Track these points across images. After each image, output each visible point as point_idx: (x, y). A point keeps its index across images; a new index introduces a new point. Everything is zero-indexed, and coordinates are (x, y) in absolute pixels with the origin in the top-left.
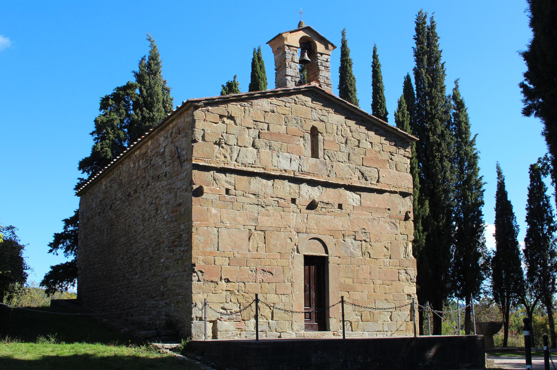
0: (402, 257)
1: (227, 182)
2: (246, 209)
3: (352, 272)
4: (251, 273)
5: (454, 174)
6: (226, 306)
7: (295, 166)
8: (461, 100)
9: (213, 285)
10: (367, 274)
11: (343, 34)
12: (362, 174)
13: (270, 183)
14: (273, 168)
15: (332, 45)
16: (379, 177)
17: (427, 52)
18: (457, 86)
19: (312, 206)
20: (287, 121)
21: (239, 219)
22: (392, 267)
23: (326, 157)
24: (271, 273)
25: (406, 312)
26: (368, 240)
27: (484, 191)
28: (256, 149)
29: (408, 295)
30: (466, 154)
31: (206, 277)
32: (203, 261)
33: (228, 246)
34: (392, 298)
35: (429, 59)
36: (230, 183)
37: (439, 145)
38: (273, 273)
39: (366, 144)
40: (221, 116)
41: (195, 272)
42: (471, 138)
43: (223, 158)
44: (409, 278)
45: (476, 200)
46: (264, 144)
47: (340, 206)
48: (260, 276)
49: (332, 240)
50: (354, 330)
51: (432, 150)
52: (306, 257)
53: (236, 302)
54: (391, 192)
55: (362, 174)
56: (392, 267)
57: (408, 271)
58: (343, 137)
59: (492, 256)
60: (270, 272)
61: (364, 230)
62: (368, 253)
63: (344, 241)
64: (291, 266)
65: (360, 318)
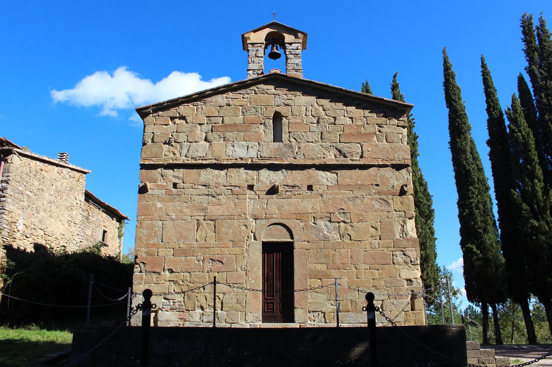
0: (398, 236)
1: (174, 177)
2: (194, 200)
3: (326, 256)
7: (253, 153)
9: (155, 276)
10: (347, 259)
11: (444, 52)
12: (340, 151)
13: (223, 173)
14: (228, 158)
15: (302, 33)
16: (362, 152)
19: (273, 191)
20: (245, 111)
21: (185, 210)
22: (382, 249)
23: (292, 140)
25: (403, 300)
28: (209, 142)
29: (407, 280)
31: (148, 268)
32: (146, 253)
35: (541, 56)
38: (224, 262)
40: (172, 119)
43: (172, 155)
44: (408, 260)
46: (217, 137)
47: (310, 188)
48: (208, 265)
50: (327, 321)
54: (379, 166)
55: (340, 151)
57: (406, 253)
58: (314, 117)
60: (219, 261)
61: (342, 211)
62: (348, 234)
63: (315, 224)
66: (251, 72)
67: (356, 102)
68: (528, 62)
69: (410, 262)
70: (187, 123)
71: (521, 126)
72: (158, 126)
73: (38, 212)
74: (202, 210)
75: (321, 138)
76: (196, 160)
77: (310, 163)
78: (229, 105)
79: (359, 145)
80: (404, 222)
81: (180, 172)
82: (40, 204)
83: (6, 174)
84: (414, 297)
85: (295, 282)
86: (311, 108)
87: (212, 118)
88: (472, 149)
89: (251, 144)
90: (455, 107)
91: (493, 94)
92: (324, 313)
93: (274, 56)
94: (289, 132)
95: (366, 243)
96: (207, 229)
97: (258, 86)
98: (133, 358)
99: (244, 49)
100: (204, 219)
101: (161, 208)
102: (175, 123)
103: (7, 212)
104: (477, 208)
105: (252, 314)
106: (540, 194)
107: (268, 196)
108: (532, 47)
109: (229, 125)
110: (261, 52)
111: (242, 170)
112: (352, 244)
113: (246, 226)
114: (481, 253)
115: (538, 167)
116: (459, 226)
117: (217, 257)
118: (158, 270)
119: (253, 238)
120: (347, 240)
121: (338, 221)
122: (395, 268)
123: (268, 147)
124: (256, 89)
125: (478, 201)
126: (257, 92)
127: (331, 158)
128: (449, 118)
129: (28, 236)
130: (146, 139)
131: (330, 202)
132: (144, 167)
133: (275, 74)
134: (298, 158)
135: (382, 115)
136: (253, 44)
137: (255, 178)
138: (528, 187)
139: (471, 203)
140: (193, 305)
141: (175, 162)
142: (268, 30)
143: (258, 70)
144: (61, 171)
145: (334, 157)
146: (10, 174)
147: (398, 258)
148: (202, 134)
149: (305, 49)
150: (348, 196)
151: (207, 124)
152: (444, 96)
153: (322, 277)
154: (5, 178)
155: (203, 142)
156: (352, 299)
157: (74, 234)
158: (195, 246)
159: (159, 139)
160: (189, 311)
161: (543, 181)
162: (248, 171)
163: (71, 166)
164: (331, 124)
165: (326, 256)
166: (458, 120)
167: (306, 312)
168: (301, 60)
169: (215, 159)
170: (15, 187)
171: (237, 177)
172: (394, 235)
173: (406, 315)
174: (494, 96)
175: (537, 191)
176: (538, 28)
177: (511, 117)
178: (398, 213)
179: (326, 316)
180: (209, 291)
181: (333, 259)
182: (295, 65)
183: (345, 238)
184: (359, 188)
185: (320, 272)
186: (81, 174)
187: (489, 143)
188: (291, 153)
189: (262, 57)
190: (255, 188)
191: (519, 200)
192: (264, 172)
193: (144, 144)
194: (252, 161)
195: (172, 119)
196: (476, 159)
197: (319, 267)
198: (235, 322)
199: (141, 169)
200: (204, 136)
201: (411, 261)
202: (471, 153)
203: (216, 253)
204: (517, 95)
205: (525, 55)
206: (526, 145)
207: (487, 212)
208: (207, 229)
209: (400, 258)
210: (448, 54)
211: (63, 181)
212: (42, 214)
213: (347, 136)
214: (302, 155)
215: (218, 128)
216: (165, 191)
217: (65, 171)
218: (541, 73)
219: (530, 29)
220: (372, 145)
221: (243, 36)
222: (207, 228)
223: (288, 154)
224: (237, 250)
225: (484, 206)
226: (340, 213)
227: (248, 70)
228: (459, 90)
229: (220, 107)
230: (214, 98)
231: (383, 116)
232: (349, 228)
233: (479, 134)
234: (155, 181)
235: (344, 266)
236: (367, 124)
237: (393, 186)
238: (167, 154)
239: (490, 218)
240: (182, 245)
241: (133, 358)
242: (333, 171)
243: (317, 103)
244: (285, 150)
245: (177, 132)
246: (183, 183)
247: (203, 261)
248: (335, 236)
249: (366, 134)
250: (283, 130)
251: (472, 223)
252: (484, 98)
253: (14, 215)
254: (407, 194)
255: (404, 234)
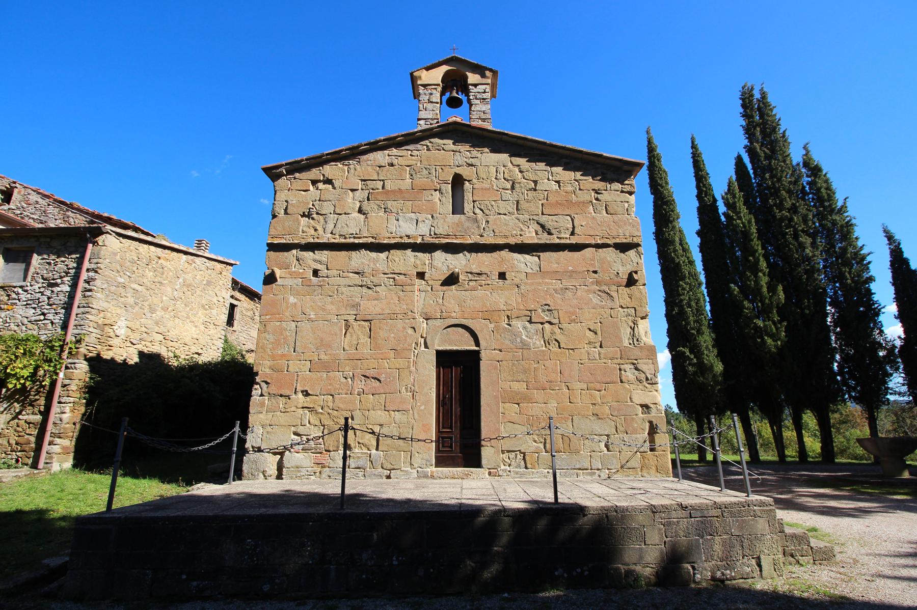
0: (626, 343)
1: (315, 261)
2: (342, 294)
3: (525, 371)
4: (345, 380)
5: (817, 249)
6: (301, 430)
7: (424, 229)
8: (817, 166)
9: (282, 401)
10: (554, 375)
11: (648, 132)
12: (543, 226)
13: (383, 256)
14: (390, 235)
15: (491, 70)
16: (574, 228)
17: (758, 125)
18: (808, 152)
19: (452, 280)
20: (413, 173)
21: (329, 307)
22: (604, 361)
23: (477, 211)
24: (379, 380)
25: (638, 436)
26: (556, 321)
27: (869, 263)
28: (364, 214)
29: (642, 406)
30: (834, 223)
31: (273, 389)
32: (270, 368)
33: (310, 346)
34: (608, 411)
35: (763, 132)
36: (320, 262)
37: (791, 220)
38: (382, 379)
39: (544, 184)
40: (314, 182)
41: (257, 383)
42: (839, 204)
43: (313, 232)
44: (643, 376)
45: (859, 276)
46: (376, 207)
47: (502, 276)
48: (360, 384)
49: (487, 326)
50: (529, 466)
51: (781, 227)
52: (439, 353)
53: (318, 423)
54: (598, 246)
55: (543, 226)
56: (604, 361)
57: (639, 366)
58: (508, 180)
59: (898, 343)
60: (375, 378)
61: (547, 307)
62: (556, 340)
63: (509, 325)
64: (413, 369)
65: (542, 446)
66: (422, 122)
67: (564, 160)
70: (334, 188)
71: (740, 212)
72: (294, 192)
73: (152, 310)
75: (517, 209)
77: (501, 241)
78: (392, 165)
79: (569, 218)
81: (324, 255)
82: (156, 301)
83: (95, 261)
84: (653, 430)
87: (368, 182)
89: (421, 217)
90: (662, 193)
92: (524, 454)
93: (454, 103)
97: (432, 140)
98: (184, 577)
99: (415, 98)
103: (93, 311)
104: (690, 306)
106: (765, 289)
107: (445, 288)
110: (436, 97)
111: (409, 252)
116: (666, 326)
120: (554, 348)
122: (625, 388)
127: (531, 236)
130: (277, 209)
131: (530, 295)
132: (272, 247)
133: (455, 123)
136: (425, 86)
139: (682, 301)
140: (336, 443)
141: (317, 241)
142: (445, 68)
146: (100, 261)
154: (93, 266)
155: (356, 215)
164: (530, 190)
165: (525, 371)
170: (110, 277)
179: (527, 457)
181: (535, 375)
182: (481, 112)
184: (570, 276)
185: (517, 393)
187: (699, 233)
192: (439, 255)
193: (274, 216)
194: (423, 239)
195: (314, 182)
197: (516, 386)
202: (681, 244)
204: (734, 178)
206: (746, 234)
207: (700, 311)
210: (653, 134)
212: (160, 313)
215: (375, 195)
217: (197, 260)
218: (765, 153)
219: (751, 101)
220: (587, 217)
221: (412, 74)
224: (401, 363)
225: (697, 303)
227: (419, 120)
230: (371, 156)
231: (600, 180)
232: (557, 331)
233: (688, 223)
234: (287, 267)
238: (305, 231)
240: (323, 357)
241: (184, 577)
244: (467, 224)
247: (353, 378)
252: (694, 183)
253: (109, 315)
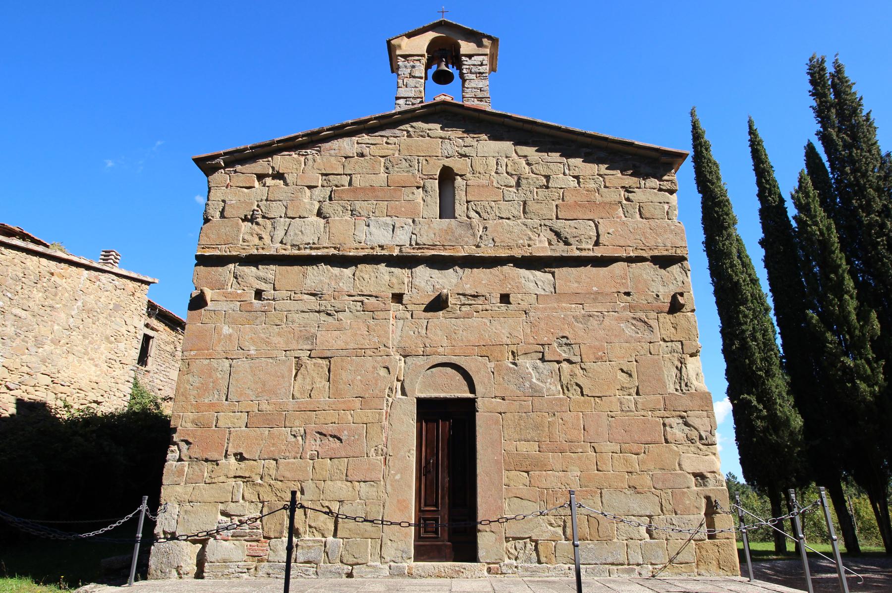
0: (671, 389)
1: (258, 278)
2: (293, 322)
3: (537, 427)
10: (576, 432)
11: (692, 114)
12: (558, 234)
13: (348, 272)
14: (358, 245)
15: (489, 38)
16: (598, 236)
19: (438, 304)
20: (390, 165)
22: (643, 413)
23: (472, 214)
25: (692, 517)
28: (324, 218)
29: (695, 475)
31: (196, 452)
32: (193, 422)
35: (839, 114)
38: (343, 438)
40: (261, 177)
43: (256, 241)
44: (694, 435)
46: (340, 209)
47: (505, 299)
48: (313, 445)
50: (543, 559)
54: (630, 260)
55: (558, 234)
57: (690, 421)
58: (511, 175)
60: (334, 437)
61: (564, 340)
62: (577, 385)
66: (401, 102)
68: (819, 125)
69: (697, 439)
71: (815, 216)
73: (39, 344)
74: (307, 338)
75: (524, 212)
76: (299, 249)
77: (503, 253)
78: (362, 155)
80: (682, 362)
81: (270, 271)
82: (44, 330)
84: (711, 508)
85: (479, 479)
86: (506, 160)
87: (331, 177)
88: (739, 252)
89: (399, 222)
90: (712, 191)
91: (768, 172)
92: (536, 542)
93: (443, 78)
94: (468, 202)
95: (611, 402)
96: (315, 375)
97: (414, 124)
99: (393, 72)
100: (309, 356)
101: (230, 335)
102: (264, 185)
104: (754, 339)
105: (395, 545)
106: (853, 317)
107: (429, 314)
108: (826, 102)
109: (361, 188)
110: (420, 70)
111: (382, 267)
112: (584, 402)
113: (388, 368)
114: (764, 408)
115: (847, 276)
117: (329, 429)
118: (214, 456)
119: (399, 392)
121: (557, 359)
122: (671, 450)
123: (429, 227)
124: (410, 129)
125: (754, 328)
126: (412, 133)
127: (542, 247)
128: (702, 208)
129: (12, 386)
132: (203, 261)
133: (444, 103)
134: (482, 245)
135: (630, 172)
136: (405, 57)
137: (406, 280)
138: (833, 306)
139: (743, 332)
140: (278, 527)
141: (262, 252)
142: (431, 35)
143: (415, 98)
144: (96, 277)
145: (547, 244)
147: (674, 430)
148: (312, 204)
149: (495, 71)
150: (575, 314)
151: (323, 186)
152: (693, 175)
153: (529, 468)
155: (314, 219)
156: (589, 513)
157: (119, 381)
158: (290, 408)
159: (234, 212)
160: (269, 538)
161: (857, 298)
162: (393, 269)
163: (116, 270)
164: (541, 187)
165: (537, 427)
166: (717, 209)
167: (501, 539)
168: (487, 83)
169: (335, 248)
171: (373, 279)
172: (664, 386)
173: (700, 548)
174: (769, 175)
175: (849, 312)
176: (832, 76)
177: (800, 203)
178: (669, 344)
179: (539, 547)
180: (311, 498)
182: (476, 90)
183: (572, 391)
184: (595, 299)
185: (526, 457)
186: (139, 284)
188: (472, 238)
189: (421, 78)
190: (406, 299)
191: (819, 327)
192: (422, 272)
193: (207, 220)
194: (401, 251)
195: (261, 177)
196: (746, 265)
197: (524, 447)
198: (360, 561)
199: (196, 265)
200: (317, 207)
201: (701, 438)
202: (739, 257)
203: (328, 421)
205: (814, 115)
206: (825, 244)
207: (768, 345)
208: (315, 375)
209: (678, 431)
210: (698, 115)
211: (100, 293)
213: (569, 207)
214: (491, 241)
215: (339, 193)
216: (239, 303)
217: (104, 277)
219: (822, 77)
221: (389, 42)
222: (315, 370)
223: (466, 239)
224: (369, 415)
225: (764, 335)
226: (560, 345)
227: (397, 98)
228: (717, 167)
229: (346, 158)
230: (335, 144)
231: (631, 175)
233: (748, 230)
235: (571, 446)
236: (605, 187)
237: (658, 296)
238: (246, 238)
239: (775, 354)
240: (264, 406)
242: (547, 270)
243: (516, 152)
244: (459, 231)
245: (267, 200)
246: (274, 289)
247: (304, 437)
248: (553, 388)
249: (603, 205)
250: (457, 197)
251: (747, 361)
254: (684, 309)
255: (683, 385)
